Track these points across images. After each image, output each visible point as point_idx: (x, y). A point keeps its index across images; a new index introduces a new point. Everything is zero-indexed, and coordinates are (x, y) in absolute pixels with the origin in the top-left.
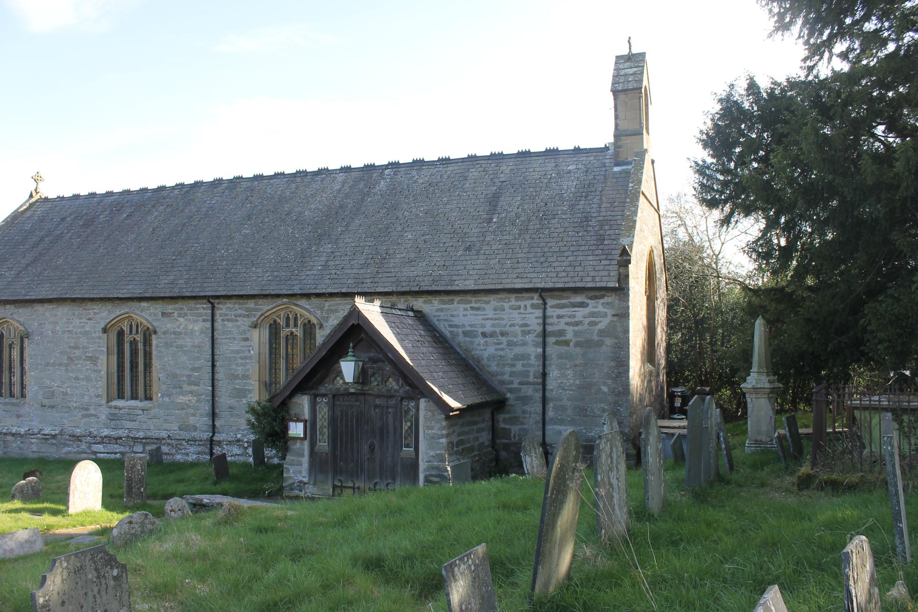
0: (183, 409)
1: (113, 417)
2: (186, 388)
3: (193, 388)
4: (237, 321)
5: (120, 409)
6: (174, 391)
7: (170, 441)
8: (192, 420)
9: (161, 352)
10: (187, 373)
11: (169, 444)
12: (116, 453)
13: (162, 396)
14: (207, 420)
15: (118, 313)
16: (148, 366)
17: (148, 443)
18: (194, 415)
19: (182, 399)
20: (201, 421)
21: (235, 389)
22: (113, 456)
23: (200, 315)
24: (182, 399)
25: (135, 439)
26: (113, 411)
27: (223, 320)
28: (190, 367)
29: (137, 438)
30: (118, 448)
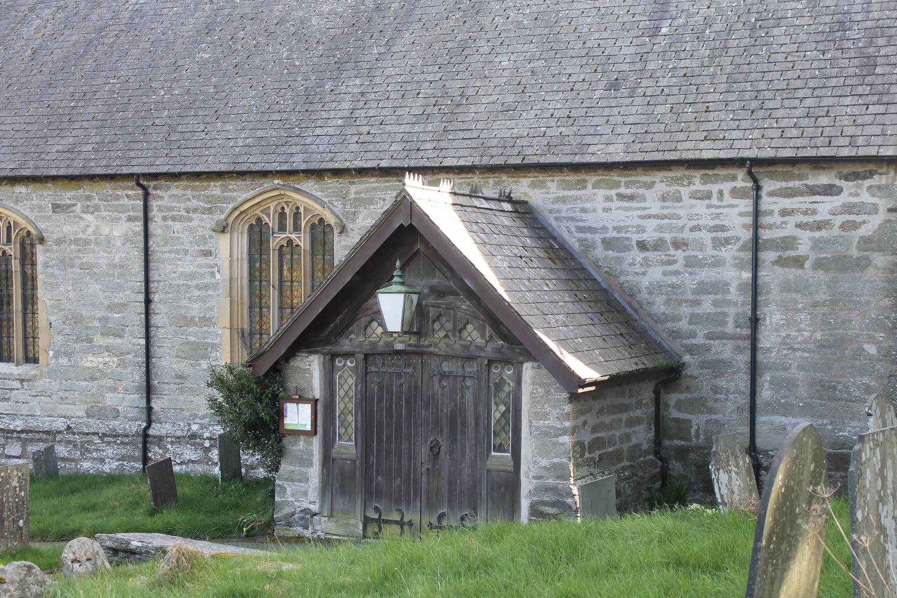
0: (94, 379)
2: (100, 340)
3: (111, 341)
7: (70, 437)
8: (111, 399)
9: (52, 275)
10: (100, 314)
11: (69, 442)
13: (56, 357)
18: (114, 390)
19: (91, 361)
20: (126, 401)
21: (188, 343)
23: (123, 209)
24: (91, 361)
28: (106, 303)
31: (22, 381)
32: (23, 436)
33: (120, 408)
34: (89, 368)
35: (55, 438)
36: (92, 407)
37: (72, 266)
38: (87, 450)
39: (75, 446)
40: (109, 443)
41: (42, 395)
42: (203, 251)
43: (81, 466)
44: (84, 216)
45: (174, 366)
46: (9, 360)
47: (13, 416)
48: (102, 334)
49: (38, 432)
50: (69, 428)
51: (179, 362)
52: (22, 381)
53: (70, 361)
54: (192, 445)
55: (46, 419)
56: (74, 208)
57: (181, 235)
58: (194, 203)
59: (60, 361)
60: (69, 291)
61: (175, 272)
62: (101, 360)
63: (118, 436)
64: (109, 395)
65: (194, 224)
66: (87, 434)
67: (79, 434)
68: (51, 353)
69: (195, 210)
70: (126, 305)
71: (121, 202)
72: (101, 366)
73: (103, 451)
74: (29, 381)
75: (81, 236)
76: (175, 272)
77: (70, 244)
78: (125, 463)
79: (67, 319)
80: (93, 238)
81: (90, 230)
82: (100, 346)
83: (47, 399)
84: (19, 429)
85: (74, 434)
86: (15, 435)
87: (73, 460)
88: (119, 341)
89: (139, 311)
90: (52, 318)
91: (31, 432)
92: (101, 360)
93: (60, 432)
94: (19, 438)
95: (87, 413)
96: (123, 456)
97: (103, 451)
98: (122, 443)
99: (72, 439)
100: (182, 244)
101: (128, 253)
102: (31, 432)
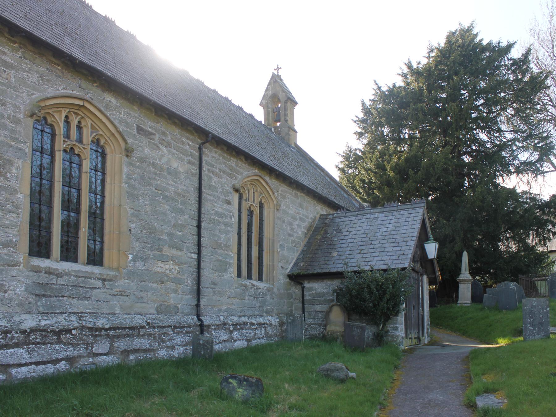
0: (162, 282)
1: (43, 291)
2: (167, 251)
3: (175, 252)
4: (221, 178)
5: (59, 275)
6: (151, 253)
7: (151, 331)
8: (172, 299)
9: (133, 187)
10: (169, 229)
11: (150, 335)
12: (57, 361)
13: (134, 260)
14: (190, 299)
15: (62, 92)
16: (40, 198)
17: (118, 337)
18: (175, 291)
19: (161, 267)
20: (182, 299)
21: (218, 260)
22: (50, 369)
23: (185, 153)
24: (161, 267)
25: (96, 331)
26: (43, 278)
27: (209, 171)
28: (173, 222)
29: (100, 329)
30: (60, 351)
31: (104, 280)
32: (112, 333)
33: (179, 306)
34: (159, 273)
35: (139, 332)
36: (161, 305)
37: (150, 185)
38: (163, 341)
39: (154, 338)
40: (178, 333)
41: (121, 295)
42: (227, 200)
43: (159, 354)
44: (160, 146)
45: (211, 275)
46: (75, 260)
47: (95, 315)
48: (169, 246)
49: (125, 328)
50: (148, 323)
51: (213, 273)
52: (104, 280)
53: (145, 265)
54: (224, 330)
55: (126, 316)
56: (153, 137)
57: (217, 186)
58: (223, 167)
59: (137, 264)
60: (146, 205)
61: (213, 210)
62: (167, 267)
63: (184, 327)
64: (172, 295)
65: (223, 181)
66: (164, 327)
67: (158, 327)
68: (130, 257)
69: (224, 172)
70: (185, 227)
71: (185, 148)
72: (167, 272)
73: (174, 340)
74: (110, 280)
75: (158, 162)
76: (213, 210)
77: (148, 165)
78: (187, 347)
79: (144, 229)
80: (165, 167)
81: (164, 160)
82: (167, 256)
83: (125, 298)
84: (107, 327)
85: (154, 328)
86: (103, 332)
87: (153, 350)
88: (179, 253)
89: (193, 232)
90: (132, 226)
91: (119, 328)
92: (167, 267)
93: (143, 327)
94: (108, 335)
95: (157, 311)
96: (187, 343)
97: (174, 340)
98: (187, 332)
99: (153, 332)
100: (217, 192)
101: (187, 187)
102: (119, 328)
